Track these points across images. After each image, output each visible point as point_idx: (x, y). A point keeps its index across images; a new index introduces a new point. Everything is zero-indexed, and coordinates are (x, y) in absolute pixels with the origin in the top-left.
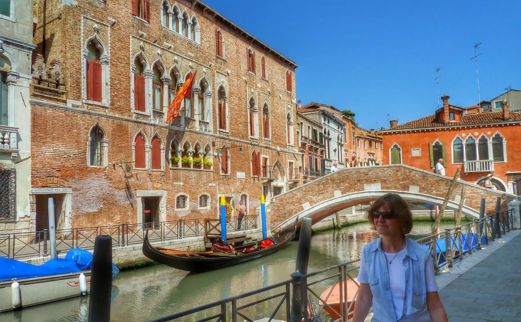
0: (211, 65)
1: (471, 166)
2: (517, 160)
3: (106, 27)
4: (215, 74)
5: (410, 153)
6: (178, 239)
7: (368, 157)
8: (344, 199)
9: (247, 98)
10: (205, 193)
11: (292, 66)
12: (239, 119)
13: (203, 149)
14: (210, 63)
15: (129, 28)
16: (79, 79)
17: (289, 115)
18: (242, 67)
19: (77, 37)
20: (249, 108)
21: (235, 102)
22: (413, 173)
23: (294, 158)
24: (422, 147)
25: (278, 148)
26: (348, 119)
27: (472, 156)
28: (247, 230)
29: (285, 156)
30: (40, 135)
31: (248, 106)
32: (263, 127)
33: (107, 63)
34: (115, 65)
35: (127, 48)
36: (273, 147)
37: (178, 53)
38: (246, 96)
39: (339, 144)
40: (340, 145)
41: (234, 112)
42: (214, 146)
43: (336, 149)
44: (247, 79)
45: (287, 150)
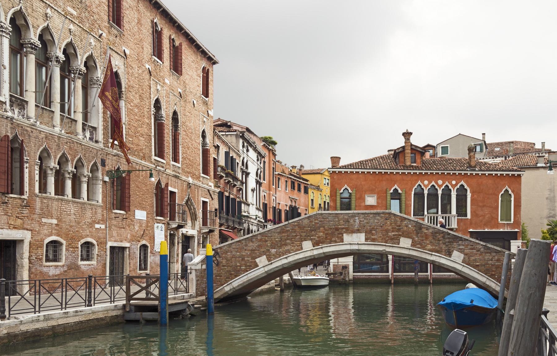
0: (101, 35)
1: (432, 220)
2: (480, 217)
5: (364, 200)
6: (111, 303)
8: (316, 252)
9: (150, 98)
10: (89, 240)
12: (139, 129)
13: (88, 168)
14: (100, 32)
17: (204, 132)
18: (144, 49)
20: (153, 114)
21: (135, 102)
22: (405, 222)
23: (209, 196)
24: (378, 194)
25: (190, 180)
26: (268, 148)
28: (177, 294)
29: (198, 191)
31: (152, 110)
32: (171, 145)
36: (184, 178)
37: (51, 3)
38: (150, 94)
40: (258, 183)
41: (132, 117)
43: (254, 189)
44: (152, 68)
45: (200, 184)
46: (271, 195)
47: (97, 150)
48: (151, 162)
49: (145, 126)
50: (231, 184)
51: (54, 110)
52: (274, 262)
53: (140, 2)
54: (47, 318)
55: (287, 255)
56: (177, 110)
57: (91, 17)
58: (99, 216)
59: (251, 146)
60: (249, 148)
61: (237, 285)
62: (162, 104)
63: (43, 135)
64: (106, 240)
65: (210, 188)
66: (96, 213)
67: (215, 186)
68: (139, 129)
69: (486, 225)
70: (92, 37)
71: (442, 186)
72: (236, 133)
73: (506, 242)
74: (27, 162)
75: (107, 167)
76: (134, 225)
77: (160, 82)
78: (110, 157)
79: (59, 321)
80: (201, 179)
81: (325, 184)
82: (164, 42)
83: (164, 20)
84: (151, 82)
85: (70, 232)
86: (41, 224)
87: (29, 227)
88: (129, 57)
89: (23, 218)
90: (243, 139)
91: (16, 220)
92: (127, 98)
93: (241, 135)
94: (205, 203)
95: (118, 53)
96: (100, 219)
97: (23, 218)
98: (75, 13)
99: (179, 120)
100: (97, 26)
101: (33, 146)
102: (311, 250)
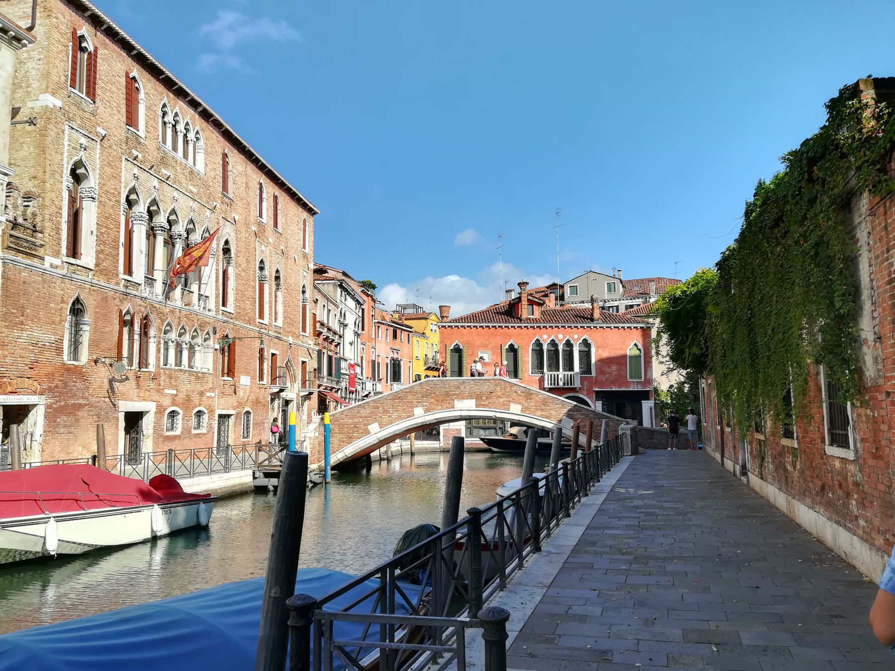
3: (94, 142)
4: (221, 221)
7: (391, 355)
11: (311, 211)
15: (121, 145)
16: (59, 223)
19: (58, 156)
25: (291, 340)
26: (367, 294)
27: (554, 366)
30: (12, 310)
31: (257, 272)
33: (94, 199)
34: (103, 203)
35: (117, 177)
39: (356, 333)
42: (215, 333)
45: (300, 342)
49: (250, 290)
59: (349, 294)
61: (349, 452)
65: (309, 346)
69: (613, 383)
71: (562, 340)
73: (213, 515)
81: (432, 330)
90: (341, 288)
98: (194, 190)
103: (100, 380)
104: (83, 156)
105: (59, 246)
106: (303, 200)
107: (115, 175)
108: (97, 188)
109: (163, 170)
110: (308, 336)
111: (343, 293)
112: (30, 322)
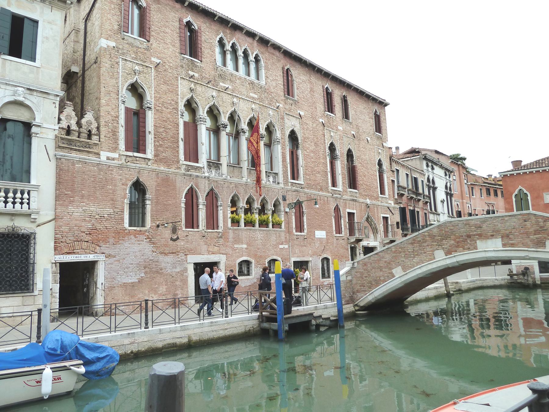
3: (149, 69)
5: (542, 198)
12: (316, 168)
14: (278, 104)
15: (176, 69)
17: (380, 161)
25: (368, 201)
26: (457, 164)
29: (377, 210)
31: (327, 152)
36: (361, 200)
37: (237, 94)
38: (325, 140)
41: (309, 160)
43: (444, 200)
45: (379, 203)
46: (465, 204)
47: (278, 189)
48: (328, 192)
49: (321, 165)
50: (415, 199)
51: (242, 166)
52: (408, 273)
53: (311, 76)
54: (183, 328)
55: (421, 264)
56: (351, 148)
57: (270, 96)
58: (283, 239)
59: (436, 164)
60: (435, 166)
62: (336, 146)
63: (233, 185)
64: (290, 257)
65: (390, 205)
66: (279, 236)
67: (395, 203)
68: (316, 168)
70: (271, 109)
72: (419, 156)
74: (221, 206)
75: (288, 201)
76: (314, 243)
77: (333, 130)
78: (290, 193)
79: (195, 330)
80: (380, 199)
82: (335, 99)
83: (335, 84)
84: (325, 132)
85: (257, 253)
86: (234, 249)
87: (223, 252)
88: (304, 117)
89: (219, 246)
91: (213, 247)
92: (303, 147)
93: (423, 157)
94: (385, 219)
95: (293, 116)
96: (284, 240)
97: (219, 246)
98: (256, 96)
99: (354, 156)
100: (275, 101)
101: (225, 194)
102: (444, 259)
103: (164, 240)
104: (138, 79)
105: (117, 144)
106: (371, 96)
107: (171, 90)
108: (153, 100)
109: (221, 84)
110: (388, 197)
111: (430, 164)
112: (86, 200)
